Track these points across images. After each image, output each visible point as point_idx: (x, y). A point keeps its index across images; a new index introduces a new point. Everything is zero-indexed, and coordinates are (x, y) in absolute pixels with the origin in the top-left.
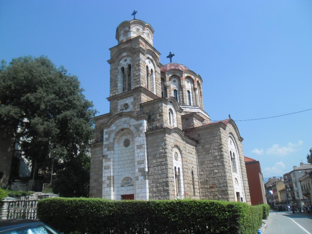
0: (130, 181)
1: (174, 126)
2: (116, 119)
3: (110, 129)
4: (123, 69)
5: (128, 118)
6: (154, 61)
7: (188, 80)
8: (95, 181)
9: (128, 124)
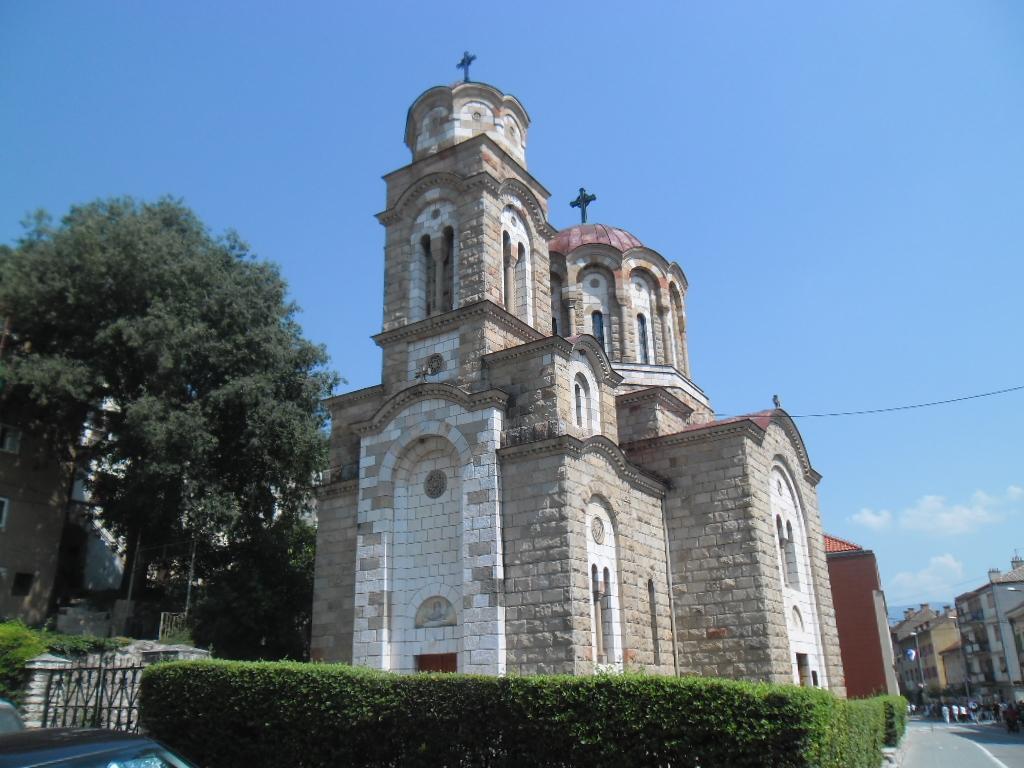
0: (443, 610)
1: (590, 430)
2: (403, 405)
3: (383, 437)
4: (426, 242)
5: (442, 403)
6: (529, 218)
7: (642, 282)
8: (331, 608)
9: (441, 421)
